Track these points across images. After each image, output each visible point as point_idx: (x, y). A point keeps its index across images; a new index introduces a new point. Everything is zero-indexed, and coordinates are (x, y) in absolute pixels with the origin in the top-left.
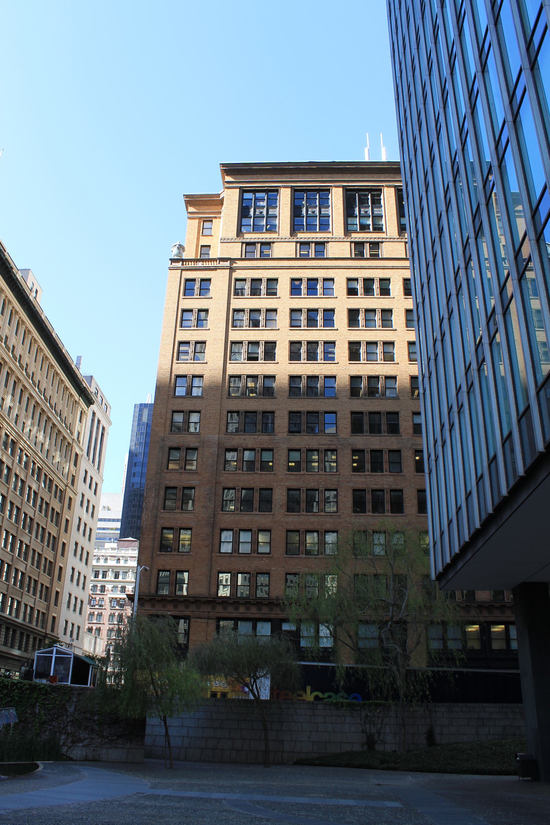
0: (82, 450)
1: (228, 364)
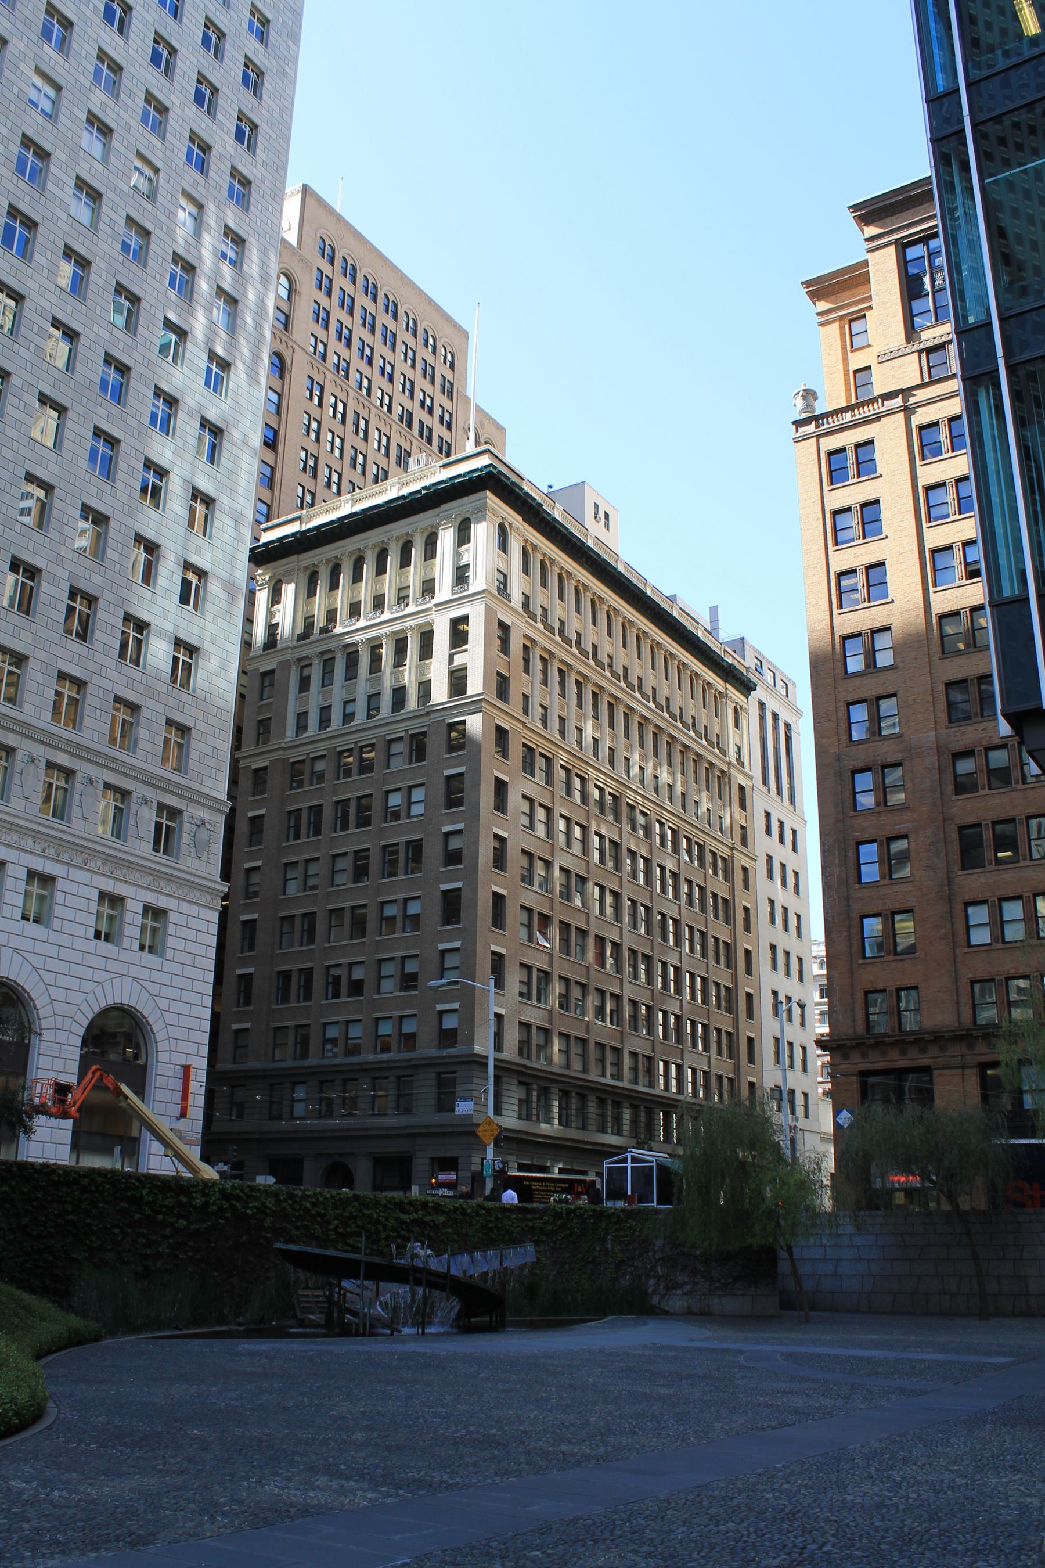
0: (751, 778)
1: (932, 595)
